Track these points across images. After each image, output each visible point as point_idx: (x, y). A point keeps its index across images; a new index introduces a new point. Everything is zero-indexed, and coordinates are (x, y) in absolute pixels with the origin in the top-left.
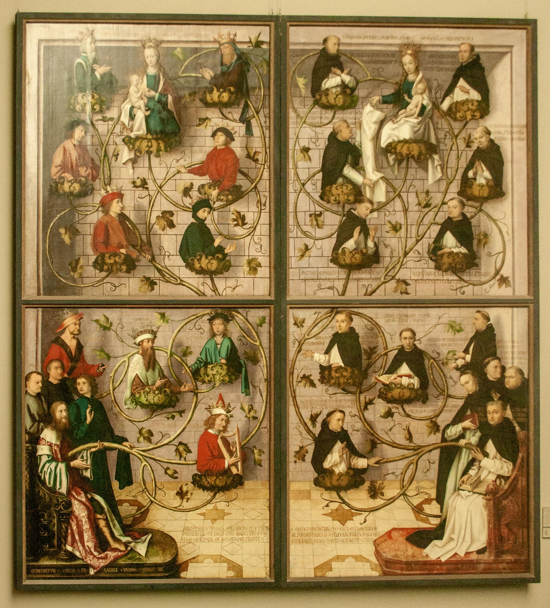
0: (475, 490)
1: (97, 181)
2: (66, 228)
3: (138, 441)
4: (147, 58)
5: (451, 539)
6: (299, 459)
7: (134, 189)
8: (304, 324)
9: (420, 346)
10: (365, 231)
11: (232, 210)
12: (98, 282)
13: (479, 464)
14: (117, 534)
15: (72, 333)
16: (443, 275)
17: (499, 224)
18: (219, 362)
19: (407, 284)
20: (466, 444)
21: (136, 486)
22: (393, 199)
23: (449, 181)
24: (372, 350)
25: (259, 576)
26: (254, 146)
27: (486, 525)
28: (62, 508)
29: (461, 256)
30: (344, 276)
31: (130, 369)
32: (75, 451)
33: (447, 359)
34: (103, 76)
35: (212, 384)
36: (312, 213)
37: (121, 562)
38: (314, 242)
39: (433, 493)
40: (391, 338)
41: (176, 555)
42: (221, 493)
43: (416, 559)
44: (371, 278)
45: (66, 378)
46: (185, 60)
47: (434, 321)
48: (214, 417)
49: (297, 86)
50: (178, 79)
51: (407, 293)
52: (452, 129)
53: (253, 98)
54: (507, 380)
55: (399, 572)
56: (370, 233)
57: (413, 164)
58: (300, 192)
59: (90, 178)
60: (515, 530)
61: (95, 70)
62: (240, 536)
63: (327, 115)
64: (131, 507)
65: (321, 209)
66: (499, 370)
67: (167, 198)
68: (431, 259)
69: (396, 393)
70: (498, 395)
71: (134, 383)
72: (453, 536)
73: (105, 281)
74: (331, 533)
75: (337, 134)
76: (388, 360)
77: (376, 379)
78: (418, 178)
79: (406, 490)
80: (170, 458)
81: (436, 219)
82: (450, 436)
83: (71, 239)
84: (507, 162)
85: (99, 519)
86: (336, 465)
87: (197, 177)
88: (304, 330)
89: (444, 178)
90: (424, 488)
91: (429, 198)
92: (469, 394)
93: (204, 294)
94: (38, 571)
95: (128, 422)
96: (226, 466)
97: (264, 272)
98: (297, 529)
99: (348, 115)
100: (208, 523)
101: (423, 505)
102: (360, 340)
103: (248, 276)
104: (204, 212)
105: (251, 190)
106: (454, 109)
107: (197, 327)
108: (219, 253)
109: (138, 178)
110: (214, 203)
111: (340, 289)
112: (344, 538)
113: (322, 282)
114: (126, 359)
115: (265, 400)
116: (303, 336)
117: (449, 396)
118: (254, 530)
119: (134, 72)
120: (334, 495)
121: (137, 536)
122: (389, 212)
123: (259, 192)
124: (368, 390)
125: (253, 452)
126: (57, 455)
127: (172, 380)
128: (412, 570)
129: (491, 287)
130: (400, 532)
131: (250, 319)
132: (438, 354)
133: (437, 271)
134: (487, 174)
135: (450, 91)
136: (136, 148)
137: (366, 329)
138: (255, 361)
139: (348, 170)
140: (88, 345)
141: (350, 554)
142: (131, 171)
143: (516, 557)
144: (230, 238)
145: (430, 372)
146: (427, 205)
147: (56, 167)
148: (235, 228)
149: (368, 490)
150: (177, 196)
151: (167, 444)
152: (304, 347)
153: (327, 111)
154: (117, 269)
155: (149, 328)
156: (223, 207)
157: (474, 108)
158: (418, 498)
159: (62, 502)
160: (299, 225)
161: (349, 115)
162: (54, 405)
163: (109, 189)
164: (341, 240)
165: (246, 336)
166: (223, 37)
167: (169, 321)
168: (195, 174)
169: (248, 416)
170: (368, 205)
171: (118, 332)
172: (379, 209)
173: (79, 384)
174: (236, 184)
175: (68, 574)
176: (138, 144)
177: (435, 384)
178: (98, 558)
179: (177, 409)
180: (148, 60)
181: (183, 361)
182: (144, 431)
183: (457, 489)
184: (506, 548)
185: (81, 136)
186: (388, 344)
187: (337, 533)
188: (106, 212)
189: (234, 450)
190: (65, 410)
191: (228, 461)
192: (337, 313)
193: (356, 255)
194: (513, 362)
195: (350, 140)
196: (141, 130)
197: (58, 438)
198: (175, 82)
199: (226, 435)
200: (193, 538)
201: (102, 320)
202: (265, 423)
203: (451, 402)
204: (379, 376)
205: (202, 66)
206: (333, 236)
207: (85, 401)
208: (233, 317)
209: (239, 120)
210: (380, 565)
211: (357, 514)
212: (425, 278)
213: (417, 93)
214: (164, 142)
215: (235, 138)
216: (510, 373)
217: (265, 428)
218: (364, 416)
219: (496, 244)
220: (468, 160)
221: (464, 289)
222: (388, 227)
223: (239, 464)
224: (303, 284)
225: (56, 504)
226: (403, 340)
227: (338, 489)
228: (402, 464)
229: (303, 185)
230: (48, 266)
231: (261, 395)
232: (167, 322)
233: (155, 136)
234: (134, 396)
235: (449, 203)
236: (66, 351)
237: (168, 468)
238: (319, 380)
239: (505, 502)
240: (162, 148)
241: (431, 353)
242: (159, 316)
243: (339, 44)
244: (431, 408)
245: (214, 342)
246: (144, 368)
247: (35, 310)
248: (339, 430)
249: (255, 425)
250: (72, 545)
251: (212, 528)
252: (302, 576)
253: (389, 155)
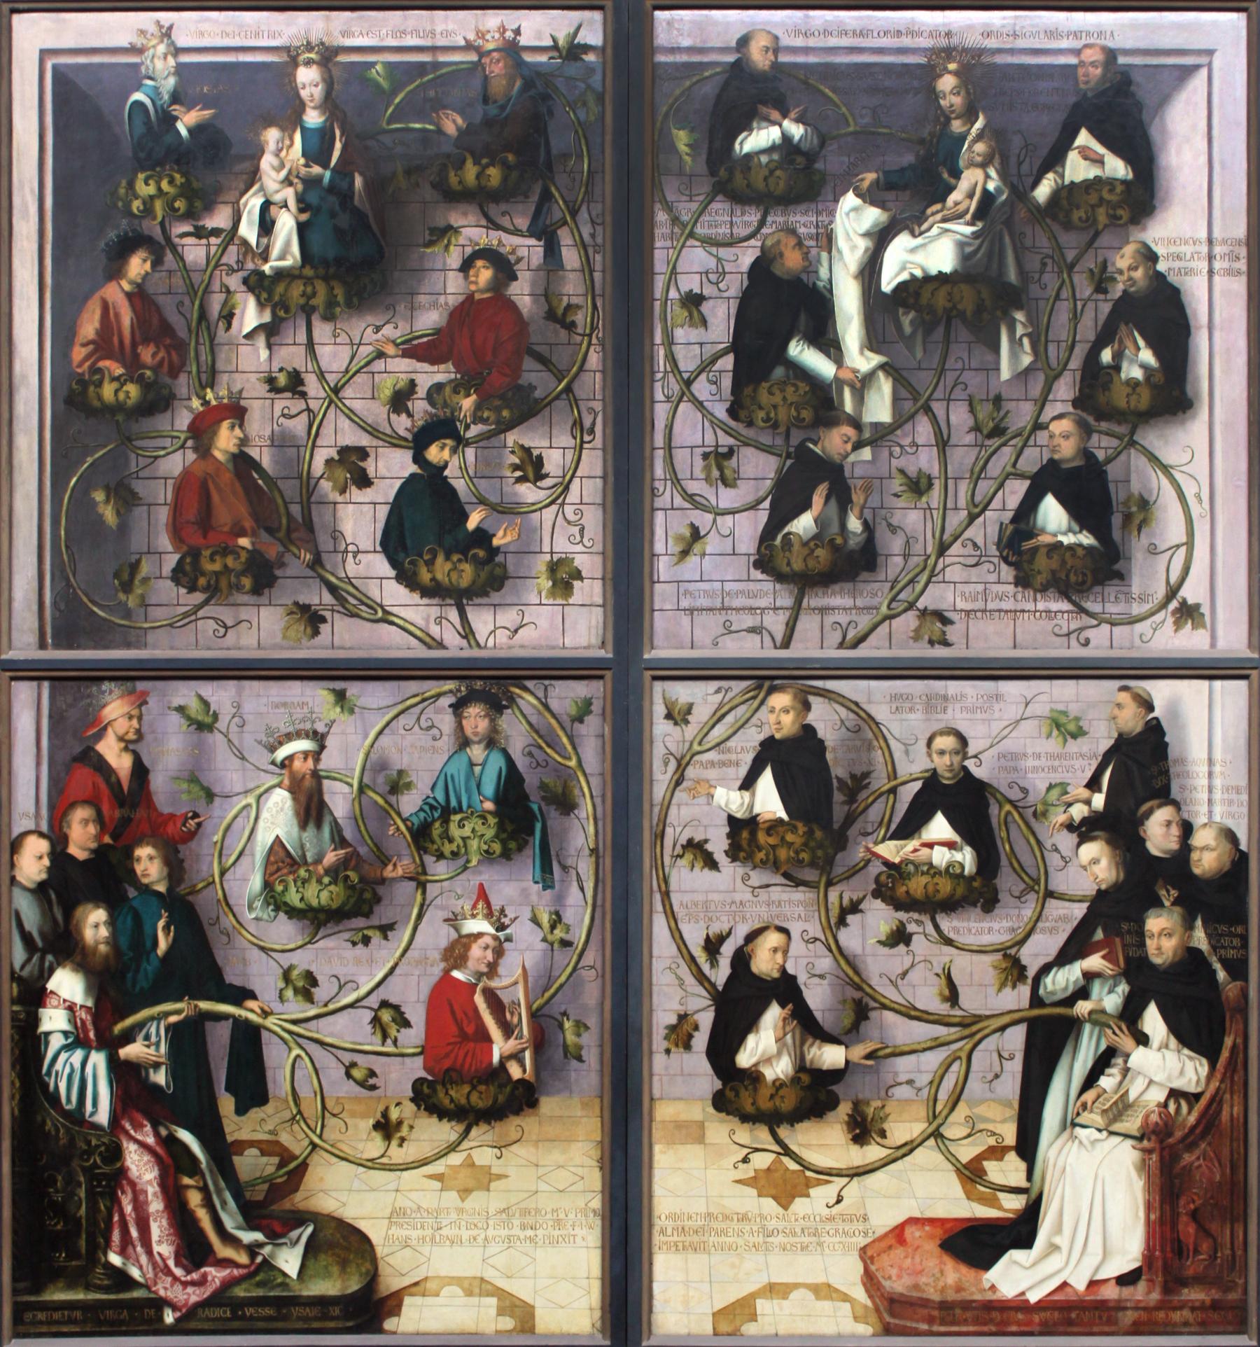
0: (1117, 1127)
1: (183, 378)
2: (108, 489)
3: (281, 997)
4: (304, 88)
5: (1053, 1248)
6: (677, 1045)
7: (272, 395)
8: (690, 718)
9: (978, 772)
10: (841, 495)
11: (510, 443)
12: (186, 615)
13: (1126, 1062)
14: (229, 1223)
15: (121, 739)
16: (1035, 600)
17: (1178, 476)
18: (479, 808)
19: (946, 621)
20: (1090, 1013)
21: (276, 1107)
22: (912, 417)
23: (1052, 374)
24: (859, 782)
25: (574, 1329)
26: (565, 292)
27: (1142, 1214)
28: (98, 1161)
29: (1080, 552)
30: (786, 600)
31: (261, 824)
32: (129, 1021)
33: (1045, 803)
34: (193, 131)
35: (461, 861)
36: (708, 450)
37: (240, 1292)
38: (715, 521)
39: (1009, 1133)
40: (907, 752)
41: (373, 1279)
42: (484, 1127)
43: (965, 1296)
44: (855, 607)
45: (108, 845)
46: (394, 93)
47: (1013, 712)
48: (464, 940)
49: (673, 148)
50: (380, 138)
51: (946, 643)
52: (1060, 248)
53: (561, 179)
54: (1195, 856)
55: (924, 1327)
56: (854, 497)
57: (963, 333)
58: (680, 401)
59: (166, 368)
60: (1214, 1227)
61: (176, 119)
62: (530, 1233)
63: (746, 218)
64: (265, 1159)
65: (731, 441)
66: (1175, 831)
67: (351, 415)
68: (1006, 560)
69: (917, 886)
70: (1174, 893)
71: (272, 859)
72: (1057, 1240)
73: (201, 614)
74: (755, 1228)
75: (772, 260)
76: (897, 805)
77: (868, 850)
78: (973, 365)
79: (942, 1124)
80: (361, 1040)
81: (1018, 466)
82: (1053, 993)
83: (118, 513)
84: (1199, 328)
85: (188, 1187)
86: (768, 1060)
87: (426, 367)
88: (691, 731)
89: (1039, 365)
90: (987, 1120)
91: (1002, 413)
92: (1099, 891)
93: (441, 645)
94: (41, 1316)
95: (256, 951)
96: (496, 1058)
97: (590, 590)
98: (672, 1217)
99: (798, 218)
100: (451, 1197)
101: (985, 1163)
102: (829, 756)
103: (551, 601)
104: (442, 448)
105: (557, 397)
106: (1065, 202)
107: (424, 724)
108: (480, 547)
109: (281, 370)
110: (467, 427)
111: (779, 631)
112: (786, 1240)
113: (733, 616)
114: (251, 799)
115: (590, 901)
116: (687, 745)
117: (1050, 894)
118: (562, 1216)
119: (269, 122)
120: (762, 1135)
121: (278, 1228)
122: (902, 447)
123: (576, 400)
124: (848, 878)
125: (561, 1026)
126: (86, 1031)
127: (363, 850)
128: (953, 1323)
129: (1155, 630)
130: (927, 1228)
131: (554, 704)
132: (1025, 791)
133: (1020, 589)
134: (1147, 356)
135: (1055, 159)
136: (277, 298)
137: (844, 729)
138: (566, 805)
139: (799, 348)
140: (160, 767)
141: (800, 1281)
142: (264, 354)
143: (1215, 1294)
144: (506, 509)
145: (1004, 834)
146: (998, 431)
147: (84, 345)
148: (517, 486)
149: (848, 1124)
150: (377, 412)
151: (351, 1006)
152: (691, 772)
153: (747, 208)
154: (230, 586)
155: (308, 726)
156: (488, 438)
157: (1113, 198)
158: (973, 1144)
159: (97, 1146)
160: (676, 481)
161: (803, 221)
162: (80, 911)
163: (210, 395)
164: (780, 517)
165: (544, 745)
166: (488, 37)
167: (356, 710)
168: (420, 359)
169: (550, 937)
170: (848, 431)
171: (230, 736)
172: (876, 440)
173: (139, 860)
174: (520, 382)
175: (112, 1323)
176: (280, 289)
177: (1016, 865)
178: (185, 1284)
179: (375, 921)
180: (304, 94)
181: (391, 806)
182: (295, 974)
183: (1070, 1124)
184: (1190, 1272)
185: (143, 272)
186: (898, 767)
187: (771, 1228)
188: (204, 450)
189: (515, 1020)
190: (105, 923)
191: (499, 1047)
192: (772, 690)
193: (820, 552)
194: (1210, 812)
195: (804, 277)
196: (289, 257)
197: (89, 989)
198: (370, 143)
199: (494, 984)
200: (415, 1234)
201: (194, 706)
202: (591, 957)
203: (1055, 908)
204: (876, 843)
205: (439, 105)
206: (761, 506)
207: (154, 901)
208: (512, 700)
209: (528, 230)
210: (877, 1310)
211: (820, 1183)
212: (991, 606)
213: (972, 164)
214: (345, 283)
215: (519, 273)
216: (1203, 837)
217: (592, 967)
218: (837, 942)
219: (1170, 525)
220: (1100, 323)
221: (1090, 633)
222: (897, 485)
223: (527, 1054)
224: (686, 620)
225: (85, 1152)
226: (935, 756)
227: (772, 1120)
228: (933, 1060)
229: (688, 383)
230: (68, 580)
231: (582, 889)
232: (352, 711)
233: (322, 271)
234: (272, 890)
235: (1051, 427)
236: (108, 781)
237: (354, 1065)
238: (726, 852)
239: (1187, 1158)
240: (340, 298)
241: (1004, 789)
242: (331, 698)
243: (776, 51)
244: (1006, 924)
245: (465, 760)
246: (295, 822)
247: (35, 684)
248: (776, 975)
249: (564, 959)
250: (122, 1252)
251: (460, 1211)
252: (683, 1331)
253: (901, 311)
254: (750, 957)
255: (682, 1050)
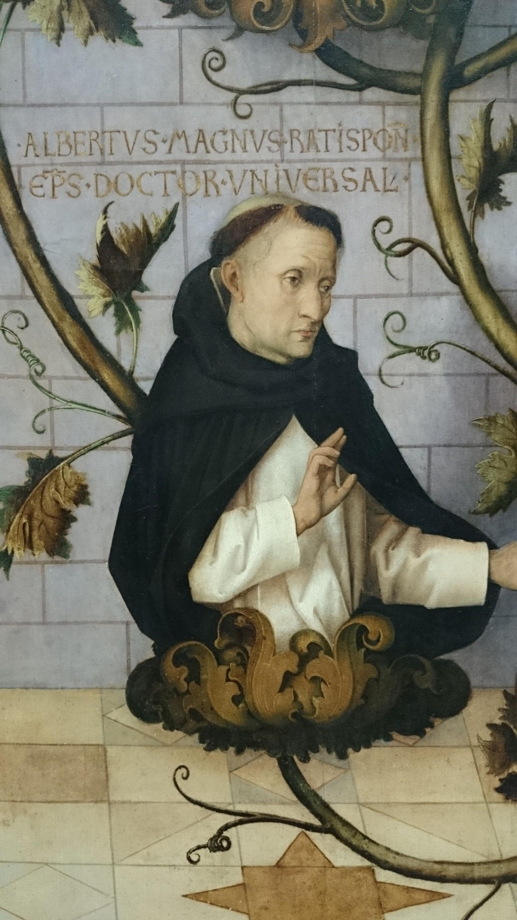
6: (29, 544)
254: (227, 296)
255: (43, 556)
